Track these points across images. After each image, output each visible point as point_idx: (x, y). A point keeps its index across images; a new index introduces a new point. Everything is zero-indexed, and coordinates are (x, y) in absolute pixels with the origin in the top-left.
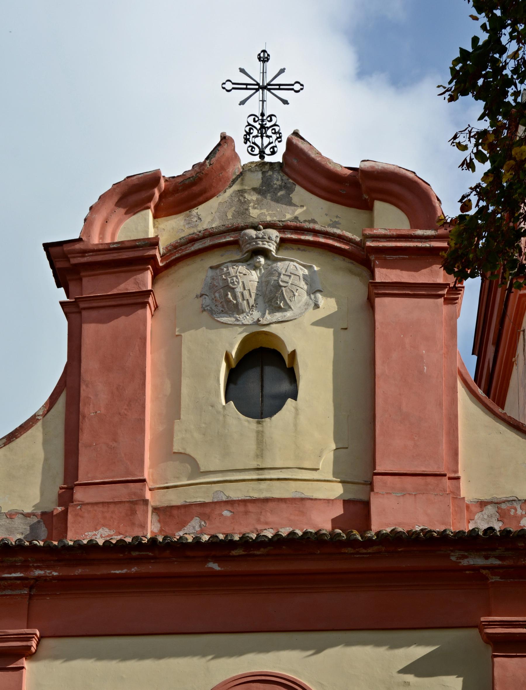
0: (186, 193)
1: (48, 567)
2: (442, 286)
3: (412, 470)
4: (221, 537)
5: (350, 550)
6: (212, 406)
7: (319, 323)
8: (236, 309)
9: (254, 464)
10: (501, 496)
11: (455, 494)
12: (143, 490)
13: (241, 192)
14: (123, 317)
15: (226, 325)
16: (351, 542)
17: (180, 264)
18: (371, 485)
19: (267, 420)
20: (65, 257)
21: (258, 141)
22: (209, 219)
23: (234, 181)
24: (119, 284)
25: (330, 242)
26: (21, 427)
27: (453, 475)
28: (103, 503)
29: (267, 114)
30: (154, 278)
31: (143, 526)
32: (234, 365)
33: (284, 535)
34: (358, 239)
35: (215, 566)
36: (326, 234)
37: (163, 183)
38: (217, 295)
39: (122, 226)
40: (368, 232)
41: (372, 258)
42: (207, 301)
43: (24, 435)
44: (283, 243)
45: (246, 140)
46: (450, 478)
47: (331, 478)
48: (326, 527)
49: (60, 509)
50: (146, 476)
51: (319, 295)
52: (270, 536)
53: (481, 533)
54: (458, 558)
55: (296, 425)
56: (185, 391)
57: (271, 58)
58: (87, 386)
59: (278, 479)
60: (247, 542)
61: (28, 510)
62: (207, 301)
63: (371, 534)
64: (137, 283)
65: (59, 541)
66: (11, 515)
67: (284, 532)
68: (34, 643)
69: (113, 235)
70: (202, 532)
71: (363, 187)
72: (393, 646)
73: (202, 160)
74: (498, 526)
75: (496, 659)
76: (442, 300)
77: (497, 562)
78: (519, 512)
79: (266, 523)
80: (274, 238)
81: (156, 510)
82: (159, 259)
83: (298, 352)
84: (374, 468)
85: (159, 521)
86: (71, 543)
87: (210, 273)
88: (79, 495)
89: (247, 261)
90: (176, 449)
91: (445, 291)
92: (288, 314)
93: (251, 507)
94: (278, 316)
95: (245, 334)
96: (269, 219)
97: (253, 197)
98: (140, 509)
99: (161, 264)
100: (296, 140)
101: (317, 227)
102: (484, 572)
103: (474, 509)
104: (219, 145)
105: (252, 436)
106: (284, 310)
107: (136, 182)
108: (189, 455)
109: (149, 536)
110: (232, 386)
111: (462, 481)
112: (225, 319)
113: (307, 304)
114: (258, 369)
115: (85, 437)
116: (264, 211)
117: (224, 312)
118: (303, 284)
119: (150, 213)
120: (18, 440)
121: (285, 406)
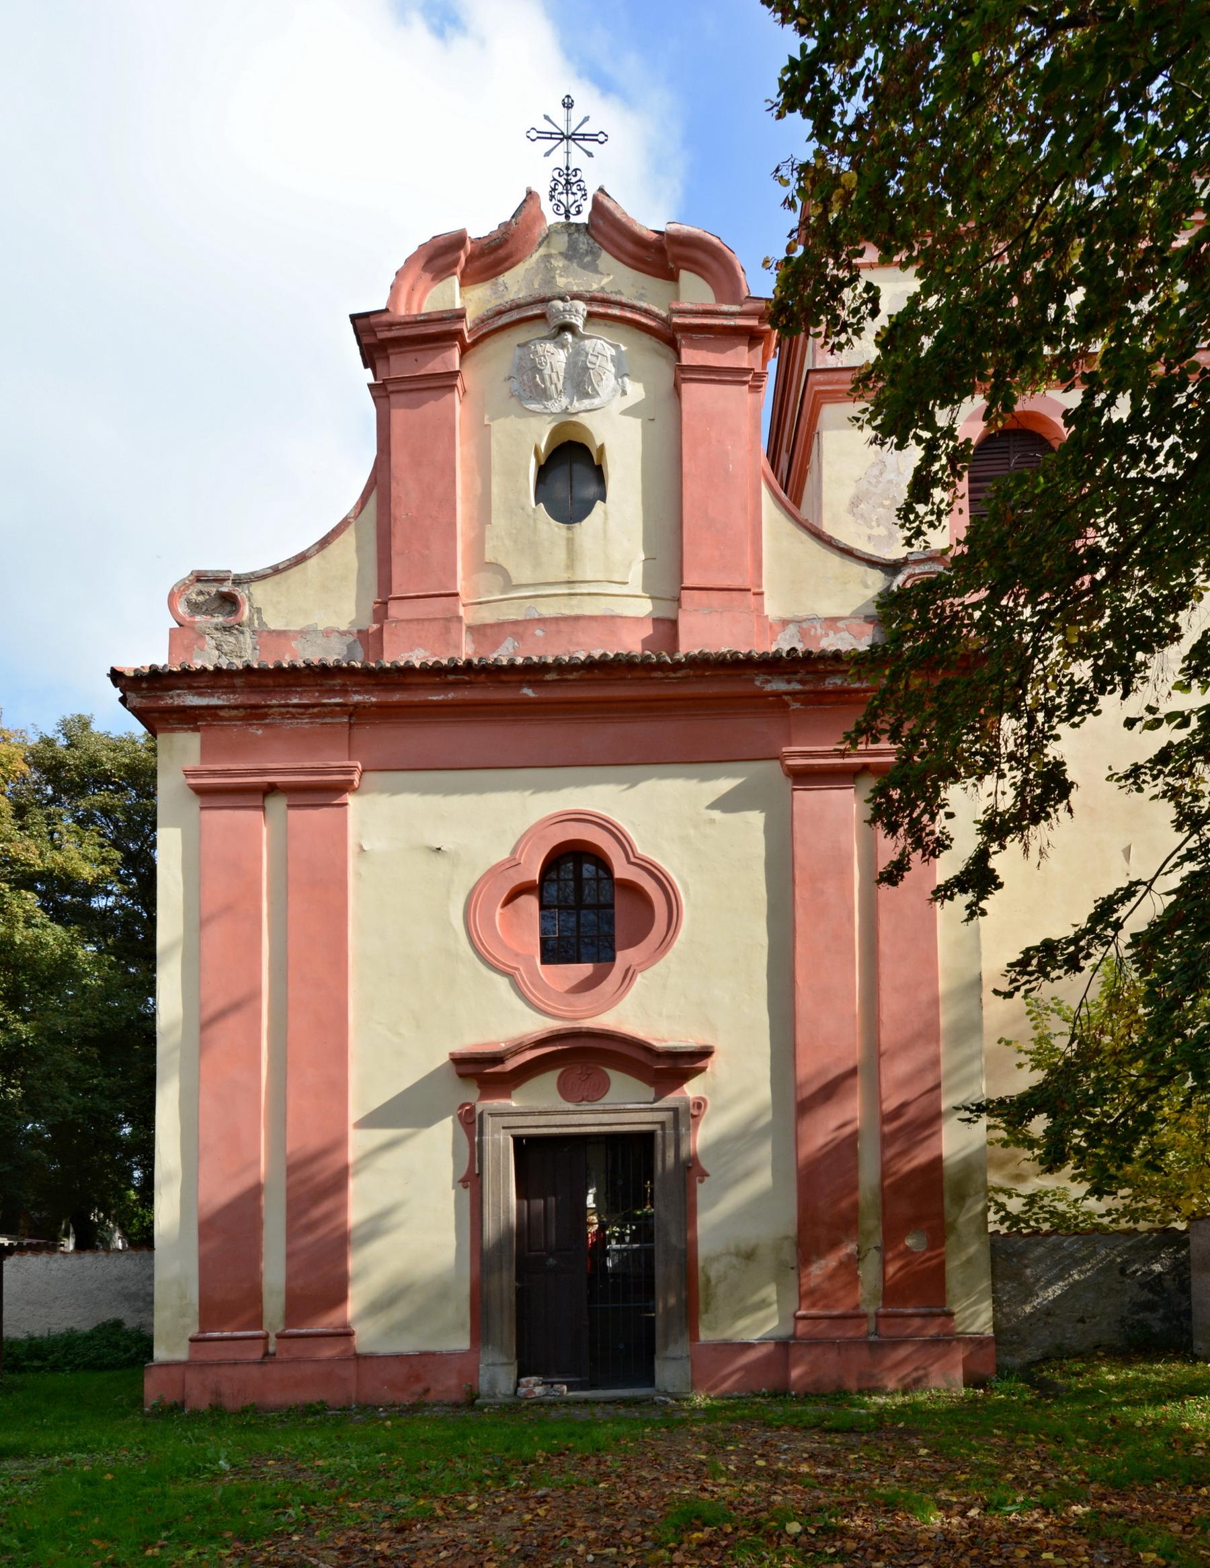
0: (492, 257)
1: (366, 692)
2: (747, 371)
3: (724, 584)
4: (535, 659)
5: (658, 674)
6: (523, 509)
7: (629, 412)
8: (543, 395)
9: (564, 576)
10: (803, 613)
12: (456, 606)
13: (548, 257)
14: (432, 402)
15: (535, 413)
16: (661, 666)
17: (488, 341)
18: (678, 600)
19: (577, 525)
20: (372, 330)
21: (563, 198)
23: (540, 245)
25: (637, 317)
26: (333, 530)
27: (757, 590)
28: (418, 620)
29: (572, 168)
30: (461, 356)
31: (458, 647)
32: (543, 463)
33: (597, 657)
34: (664, 314)
35: (529, 692)
36: (633, 308)
37: (469, 245)
38: (525, 377)
39: (428, 296)
40: (675, 306)
41: (679, 336)
42: (515, 385)
43: (337, 541)
44: (591, 315)
45: (552, 197)
46: (755, 594)
47: (640, 593)
49: (375, 626)
50: (459, 590)
51: (626, 379)
52: (583, 658)
53: (784, 655)
54: (762, 683)
55: (605, 532)
56: (495, 490)
57: (575, 104)
59: (589, 594)
60: (560, 664)
61: (344, 628)
62: (515, 385)
63: (680, 656)
64: (444, 362)
65: (377, 662)
66: (327, 633)
67: (597, 654)
68: (356, 777)
69: (420, 306)
70: (516, 654)
71: (669, 255)
72: (704, 778)
73: (508, 219)
74: (801, 647)
75: (796, 793)
76: (746, 387)
78: (819, 630)
79: (578, 644)
80: (581, 311)
81: (470, 628)
82: (466, 334)
83: (607, 447)
84: (681, 579)
85: (474, 642)
86: (388, 665)
87: (518, 351)
88: (394, 610)
89: (554, 338)
90: (489, 557)
91: (749, 378)
92: (596, 402)
93: (563, 626)
94: (586, 403)
95: (554, 424)
96: (575, 289)
97: (559, 263)
98: (454, 626)
99: (468, 341)
100: (601, 198)
101: (624, 299)
102: (786, 698)
103: (776, 628)
104: (525, 201)
105: (562, 543)
107: (442, 243)
109: (464, 658)
110: (541, 486)
111: (766, 596)
112: (533, 406)
113: (615, 390)
114: (567, 467)
115: (397, 544)
116: (570, 280)
117: (531, 399)
118: (611, 367)
119: (456, 280)
121: (594, 510)
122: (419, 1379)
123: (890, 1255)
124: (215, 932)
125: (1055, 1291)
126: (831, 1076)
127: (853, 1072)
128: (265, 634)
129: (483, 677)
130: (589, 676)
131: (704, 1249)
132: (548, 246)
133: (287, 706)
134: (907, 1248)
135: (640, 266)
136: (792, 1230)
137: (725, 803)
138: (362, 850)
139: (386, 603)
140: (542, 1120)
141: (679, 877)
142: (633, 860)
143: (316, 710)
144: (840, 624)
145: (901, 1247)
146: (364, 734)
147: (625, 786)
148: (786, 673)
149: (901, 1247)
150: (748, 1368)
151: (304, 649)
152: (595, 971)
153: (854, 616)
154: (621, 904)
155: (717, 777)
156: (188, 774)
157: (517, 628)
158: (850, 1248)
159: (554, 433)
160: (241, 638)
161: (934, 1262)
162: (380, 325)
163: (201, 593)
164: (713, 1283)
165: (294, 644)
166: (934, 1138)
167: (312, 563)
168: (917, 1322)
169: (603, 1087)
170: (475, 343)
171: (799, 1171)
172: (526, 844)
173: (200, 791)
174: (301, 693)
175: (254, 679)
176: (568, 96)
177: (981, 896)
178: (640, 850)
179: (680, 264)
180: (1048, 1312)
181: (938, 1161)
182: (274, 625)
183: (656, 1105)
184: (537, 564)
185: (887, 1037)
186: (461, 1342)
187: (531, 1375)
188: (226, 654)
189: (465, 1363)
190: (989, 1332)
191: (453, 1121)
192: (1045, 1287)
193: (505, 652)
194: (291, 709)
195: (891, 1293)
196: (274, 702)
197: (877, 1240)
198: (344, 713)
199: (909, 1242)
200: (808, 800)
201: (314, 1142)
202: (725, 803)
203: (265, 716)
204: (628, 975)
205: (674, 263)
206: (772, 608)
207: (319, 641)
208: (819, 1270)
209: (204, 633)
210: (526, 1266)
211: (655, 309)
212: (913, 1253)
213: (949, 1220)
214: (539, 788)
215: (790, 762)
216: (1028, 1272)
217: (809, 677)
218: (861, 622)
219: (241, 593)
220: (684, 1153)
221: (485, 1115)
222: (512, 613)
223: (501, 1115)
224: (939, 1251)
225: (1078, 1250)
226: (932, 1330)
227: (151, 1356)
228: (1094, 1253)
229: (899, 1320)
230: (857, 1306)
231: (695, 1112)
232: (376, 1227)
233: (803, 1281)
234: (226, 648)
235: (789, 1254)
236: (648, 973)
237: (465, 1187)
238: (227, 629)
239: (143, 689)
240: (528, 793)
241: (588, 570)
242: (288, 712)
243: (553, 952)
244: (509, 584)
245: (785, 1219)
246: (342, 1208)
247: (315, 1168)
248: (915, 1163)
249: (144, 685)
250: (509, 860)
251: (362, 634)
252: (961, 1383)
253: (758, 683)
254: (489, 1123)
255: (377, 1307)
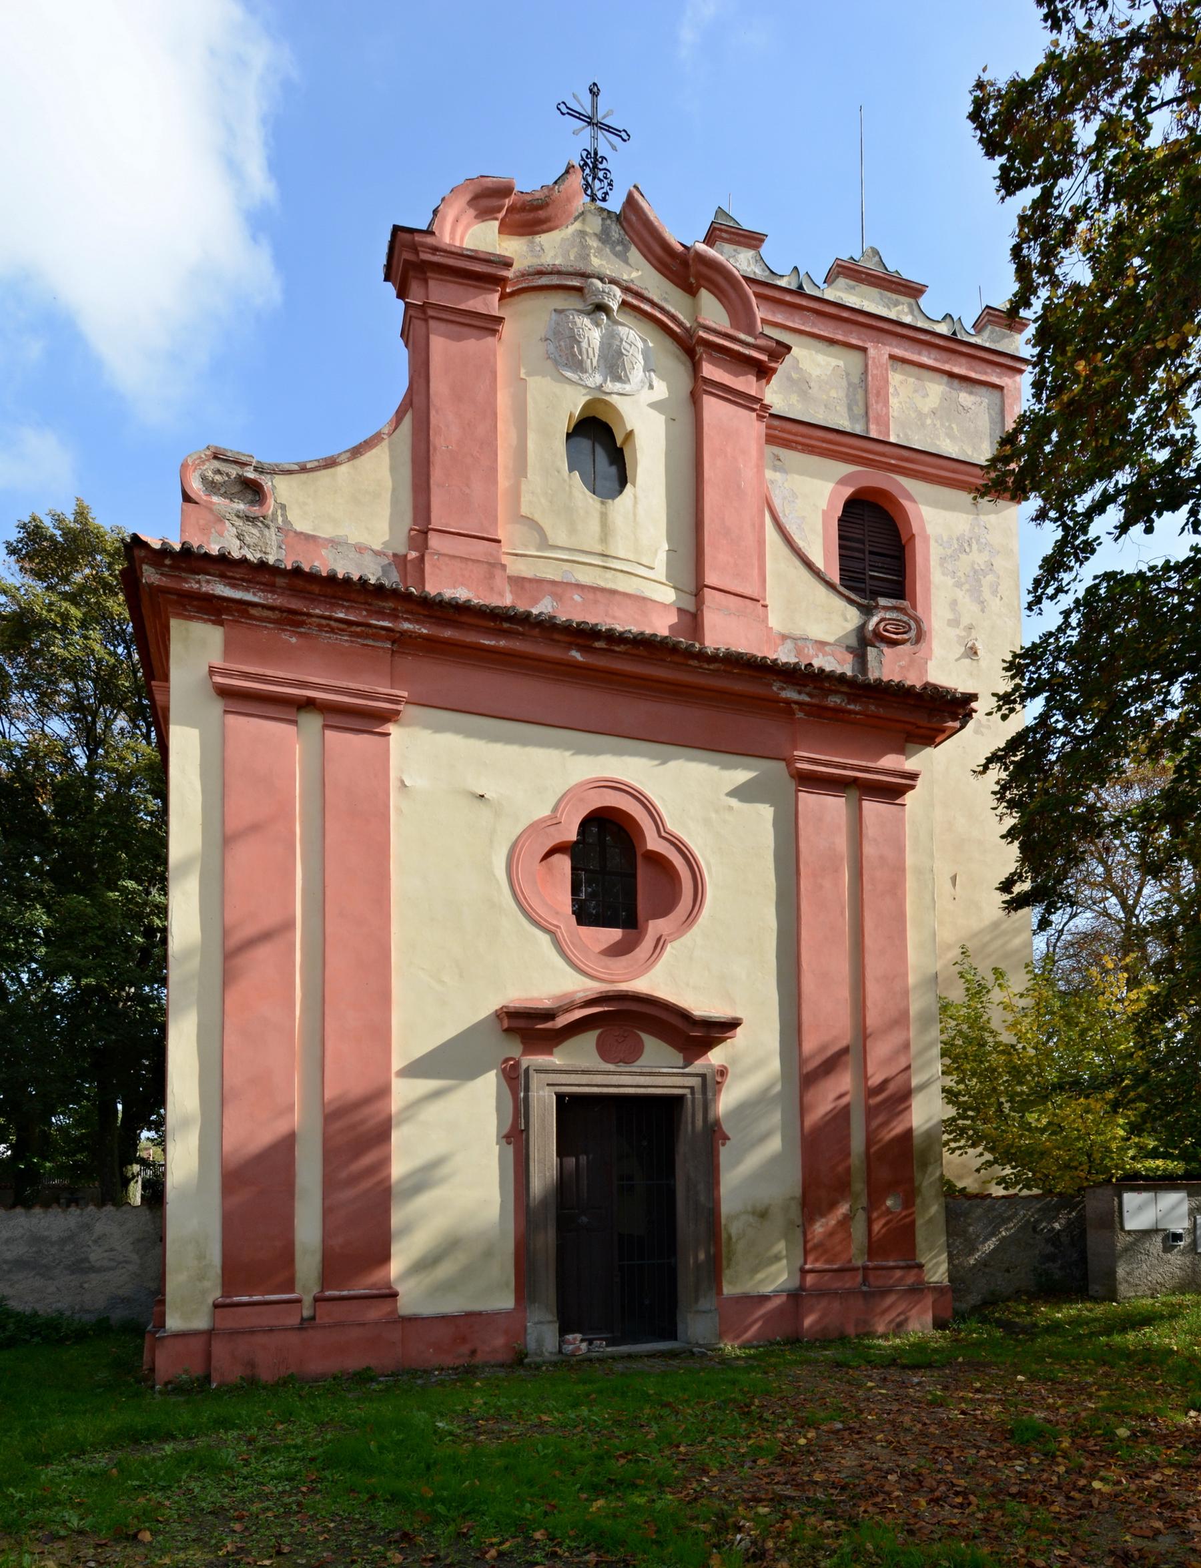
1: (417, 622)
3: (739, 590)
5: (694, 663)
7: (654, 406)
9: (598, 548)
11: (765, 620)
13: (582, 233)
14: (473, 340)
17: (524, 296)
20: (414, 248)
22: (552, 253)
23: (576, 219)
24: (468, 300)
25: (665, 319)
28: (461, 558)
35: (577, 655)
39: (470, 231)
43: (369, 454)
47: (664, 580)
48: (663, 631)
49: (413, 555)
55: (635, 515)
58: (437, 412)
59: (622, 571)
61: (377, 547)
64: (486, 304)
69: (462, 239)
71: (692, 270)
72: (725, 767)
75: (800, 794)
76: (754, 414)
77: (807, 699)
83: (636, 432)
91: (757, 407)
92: (627, 388)
94: (618, 387)
95: (588, 398)
97: (594, 243)
100: (637, 195)
102: (795, 706)
106: (623, 382)
108: (537, 523)
112: (569, 374)
113: (642, 381)
115: (437, 474)
119: (496, 224)
120: (362, 458)
122: (464, 1340)
123: (875, 1215)
124: (243, 853)
125: (991, 1244)
126: (829, 1053)
127: (845, 1051)
128: (292, 534)
129: (536, 631)
130: (635, 652)
131: (727, 1207)
132: (584, 221)
133: (330, 618)
134: (888, 1209)
135: (663, 270)
136: (798, 1192)
137: (742, 793)
138: (403, 785)
139: (426, 533)
140: (584, 1079)
141: (703, 856)
142: (663, 834)
143: (359, 629)
144: (827, 648)
145: (884, 1208)
146: (407, 663)
147: (656, 762)
148: (797, 684)
149: (884, 1208)
150: (769, 1318)
151: (335, 560)
152: (624, 936)
153: (838, 642)
154: (643, 874)
155: (735, 767)
156: (212, 671)
157: (558, 588)
158: (843, 1209)
159: (587, 406)
160: (266, 532)
161: (908, 1220)
162: (423, 245)
163: (219, 472)
164: (734, 1240)
165: (324, 552)
166: (907, 1113)
167: (343, 470)
168: (898, 1273)
169: (635, 1052)
170: (512, 294)
171: (803, 1137)
172: (567, 804)
173: (224, 693)
174: (347, 608)
175: (300, 583)
176: (595, 84)
177: (1048, 911)
178: (670, 826)
179: (702, 282)
180: (984, 1263)
181: (909, 1132)
182: (300, 526)
183: (687, 1070)
184: (572, 530)
185: (873, 1019)
186: (505, 1301)
187: (573, 1332)
188: (249, 547)
189: (512, 1322)
190: (946, 1282)
191: (497, 1075)
192: (983, 1243)
193: (543, 607)
194: (332, 623)
195: (874, 1248)
196: (317, 611)
197: (864, 1201)
198: (387, 639)
199: (889, 1203)
200: (810, 801)
201: (357, 1088)
202: (742, 793)
203: (301, 624)
204: (659, 944)
205: (696, 279)
206: (775, 622)
207: (351, 556)
208: (819, 1228)
209: (224, 517)
210: (565, 1223)
211: (681, 317)
212: (891, 1213)
213: (917, 1184)
214: (579, 750)
215: (799, 765)
216: (971, 1229)
217: (816, 692)
218: (844, 650)
219: (266, 482)
220: (711, 1117)
221: (531, 1072)
222: (549, 572)
223: (546, 1071)
224: (910, 1211)
225: (1005, 1211)
226: (910, 1279)
227: (162, 1325)
228: (1016, 1214)
229: (884, 1272)
230: (850, 1261)
231: (719, 1079)
232: (423, 1179)
233: (809, 1237)
234: (248, 540)
235: (795, 1213)
236: (676, 944)
237: (509, 1143)
238: (250, 519)
239: (166, 566)
240: (568, 754)
241: (620, 548)
242: (328, 625)
243: (583, 916)
244: (544, 542)
245: (790, 1183)
246: (386, 1161)
247: (356, 1117)
248: (893, 1133)
249: (168, 562)
250: (550, 818)
251: (400, 561)
252: (931, 1325)
253: (775, 689)
254: (536, 1080)
255: (423, 1265)
